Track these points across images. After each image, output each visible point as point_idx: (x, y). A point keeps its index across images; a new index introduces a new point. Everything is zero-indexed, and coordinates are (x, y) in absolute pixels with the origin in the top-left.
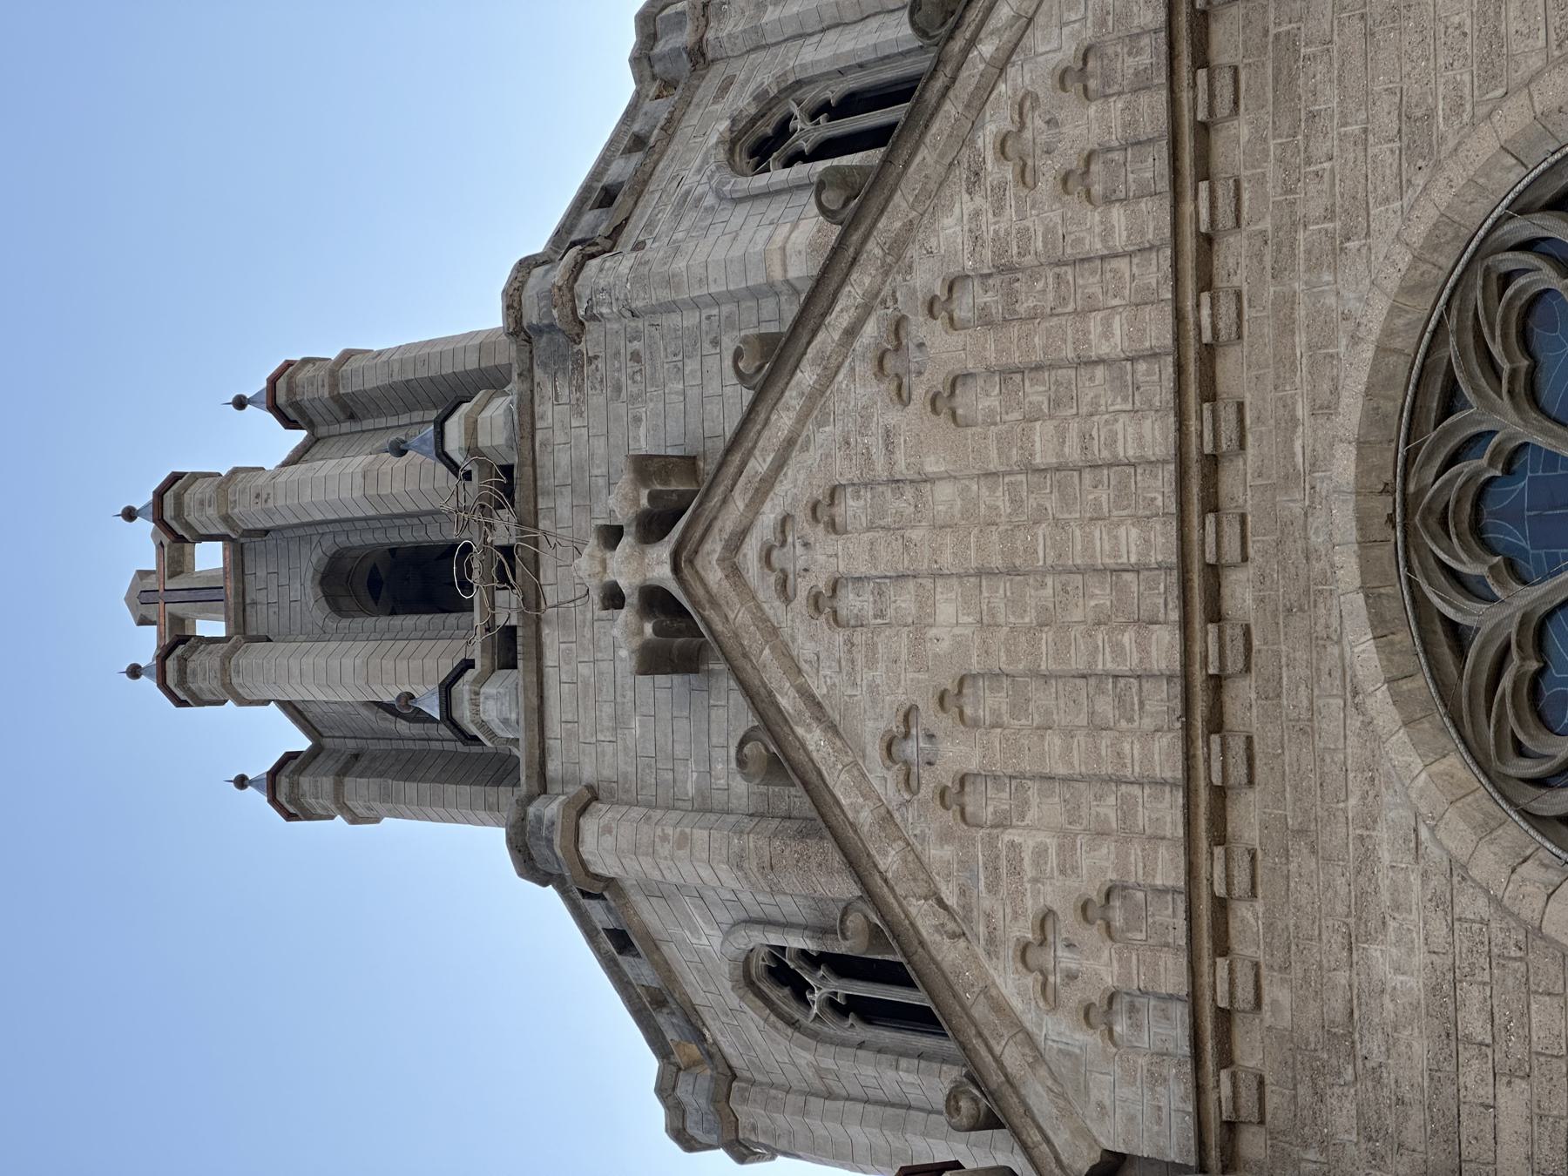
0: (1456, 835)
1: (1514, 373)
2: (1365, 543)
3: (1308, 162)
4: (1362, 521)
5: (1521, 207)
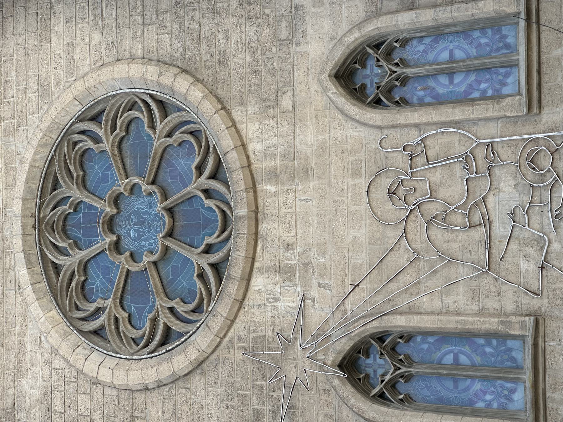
0: (54, 339)
1: (78, 176)
2: (24, 235)
3: (5, 98)
4: (24, 227)
5: (81, 119)
